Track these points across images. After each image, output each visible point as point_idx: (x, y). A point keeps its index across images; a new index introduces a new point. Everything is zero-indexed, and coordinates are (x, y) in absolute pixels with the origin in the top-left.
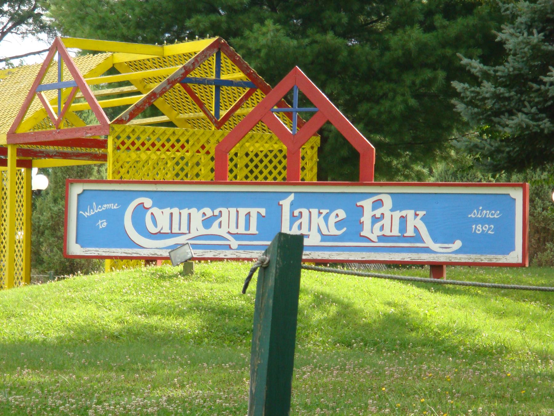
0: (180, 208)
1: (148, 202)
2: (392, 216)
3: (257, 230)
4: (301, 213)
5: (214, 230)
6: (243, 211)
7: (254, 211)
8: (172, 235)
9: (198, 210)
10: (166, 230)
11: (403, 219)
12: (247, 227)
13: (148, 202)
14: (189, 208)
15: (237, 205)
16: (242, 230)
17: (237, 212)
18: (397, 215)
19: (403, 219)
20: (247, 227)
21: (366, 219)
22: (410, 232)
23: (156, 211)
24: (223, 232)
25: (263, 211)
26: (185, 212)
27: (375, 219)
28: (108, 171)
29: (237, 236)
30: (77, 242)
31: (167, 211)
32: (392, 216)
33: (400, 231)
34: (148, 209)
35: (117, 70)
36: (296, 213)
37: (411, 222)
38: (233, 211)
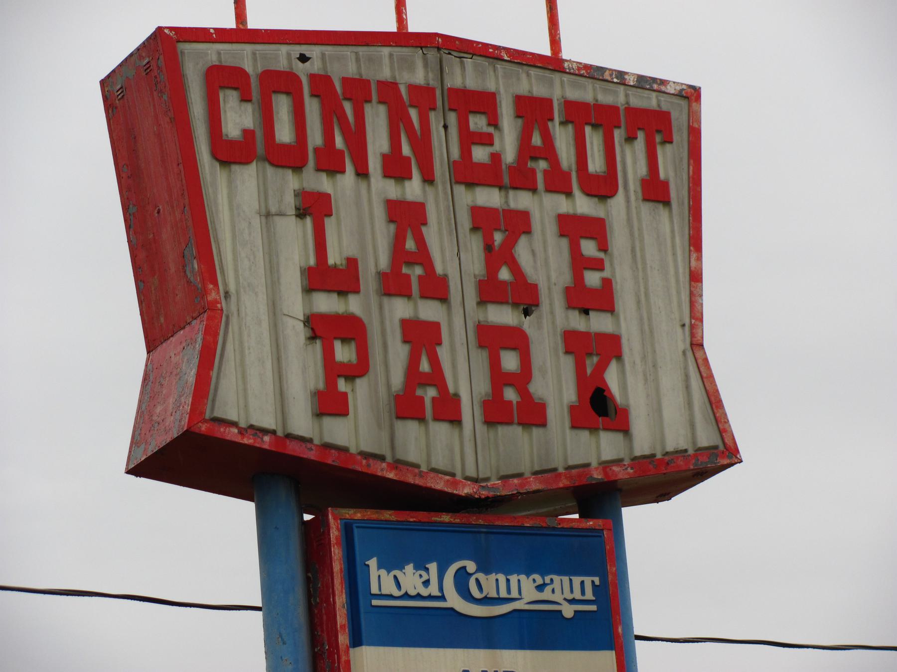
0: (507, 573)
2: (379, 576)
3: (594, 595)
4: (552, 580)
5: (546, 595)
6: (577, 580)
7: (588, 580)
9: (389, 572)
10: (494, 594)
12: (583, 592)
14: (519, 574)
16: (577, 595)
17: (571, 580)
20: (583, 592)
23: (481, 576)
24: (557, 597)
26: (514, 579)
29: (572, 601)
30: (575, 612)
31: (493, 577)
32: (379, 576)
34: (471, 575)
35: (156, 348)
38: (566, 579)
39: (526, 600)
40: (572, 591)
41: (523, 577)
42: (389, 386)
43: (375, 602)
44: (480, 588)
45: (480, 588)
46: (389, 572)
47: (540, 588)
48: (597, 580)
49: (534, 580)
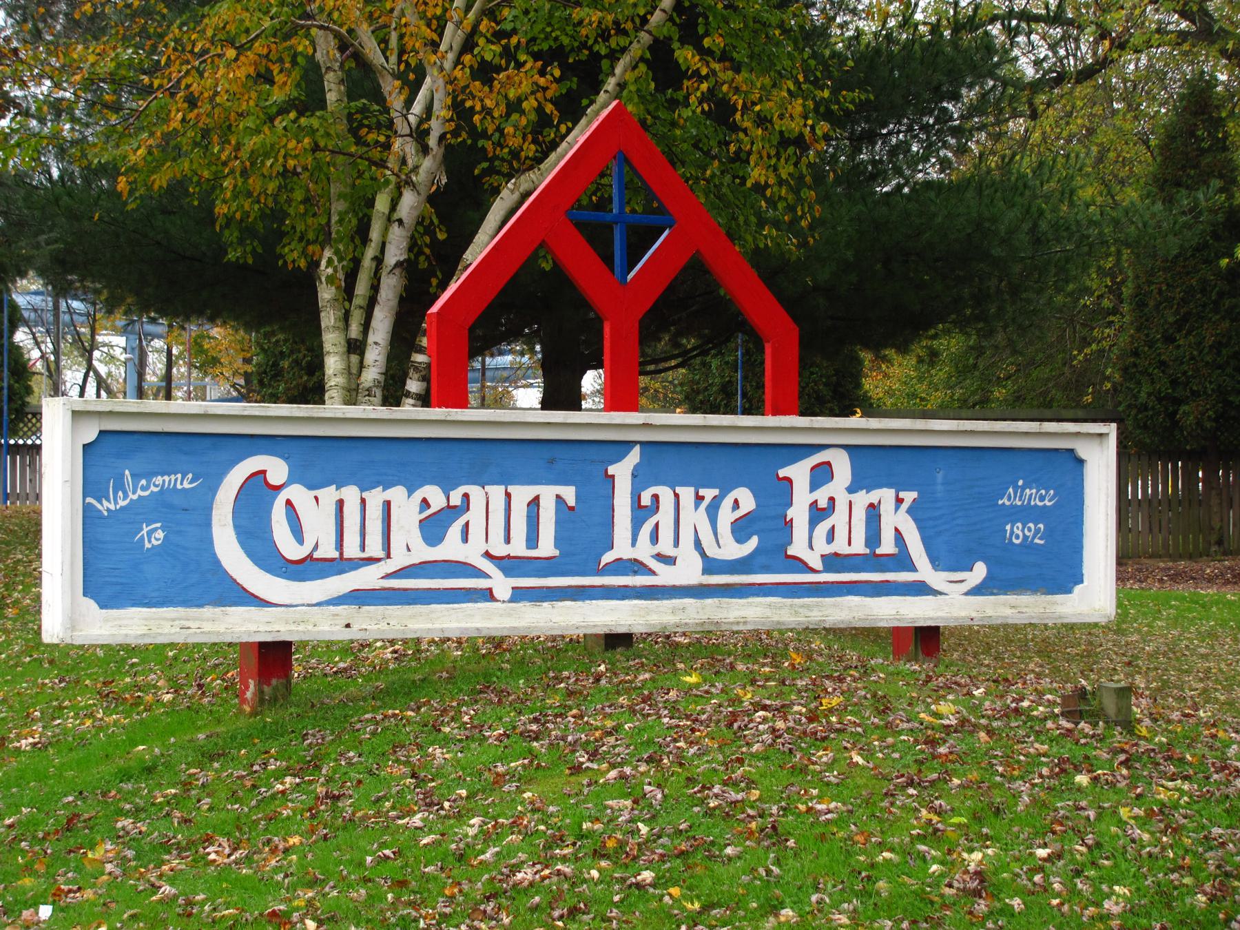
3: (556, 547)
6: (522, 494)
7: (548, 494)
8: (340, 565)
9: (410, 492)
10: (328, 550)
13: (277, 469)
17: (508, 495)
18: (862, 499)
22: (887, 546)
23: (298, 494)
24: (471, 553)
26: (376, 498)
31: (329, 495)
34: (278, 488)
39: (400, 559)
40: (508, 540)
41: (397, 494)
42: (36, 293)
43: (159, 525)
44: (298, 532)
45: (298, 532)
46: (410, 492)
47: (433, 527)
48: (569, 494)
49: (425, 503)
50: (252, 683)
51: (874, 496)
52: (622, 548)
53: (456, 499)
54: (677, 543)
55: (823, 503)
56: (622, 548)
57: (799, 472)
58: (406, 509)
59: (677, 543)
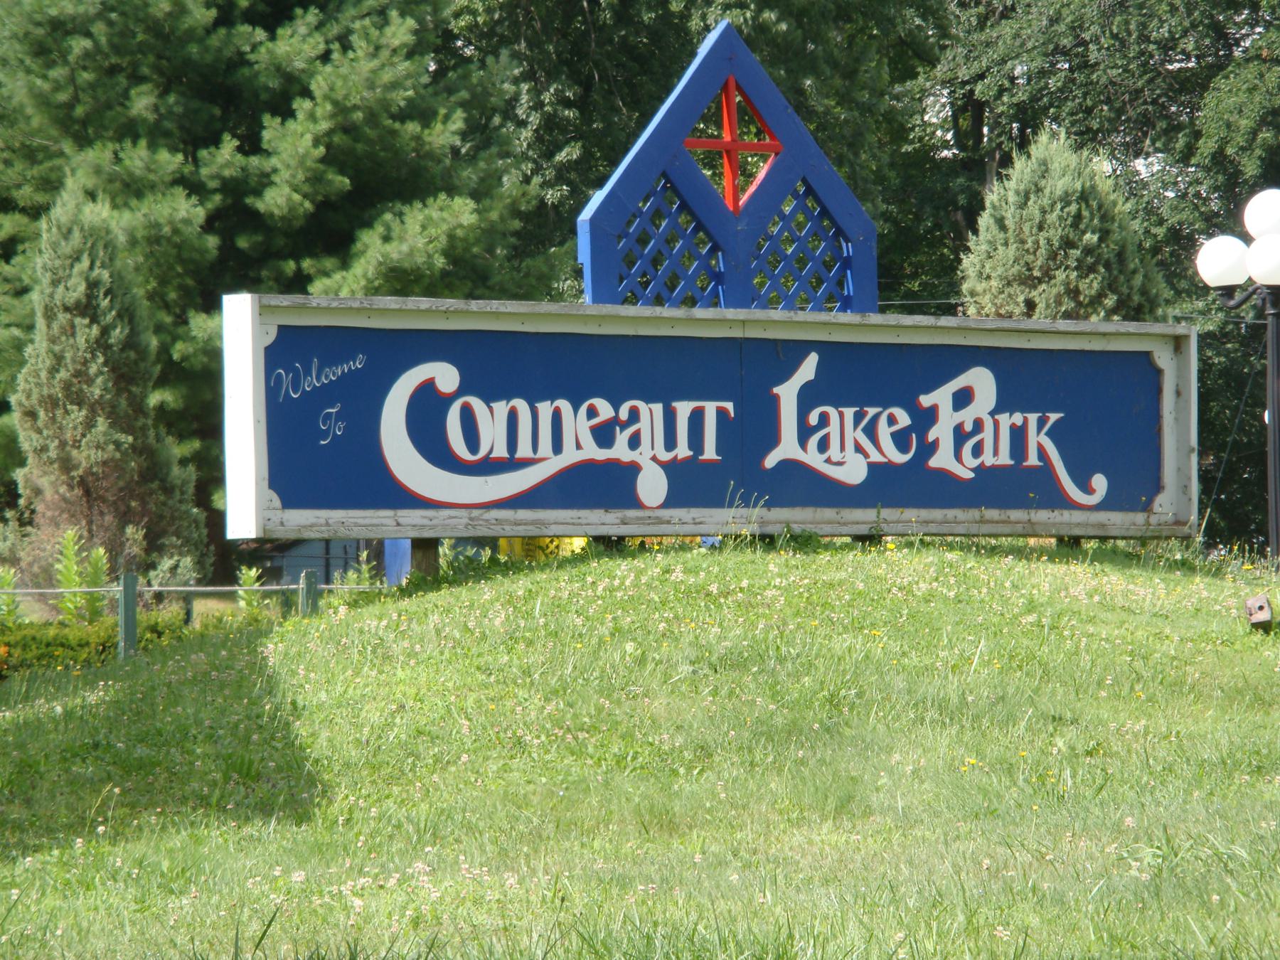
1: (446, 376)
3: (718, 454)
6: (684, 409)
7: (711, 408)
8: (512, 464)
10: (501, 451)
11: (1018, 434)
13: (446, 376)
15: (665, 395)
18: (1005, 420)
19: (1018, 434)
21: (942, 432)
22: (1033, 460)
25: (729, 406)
26: (545, 409)
27: (960, 436)
28: (614, 531)
31: (501, 408)
33: (1013, 455)
36: (813, 418)
37: (1036, 439)
50: (114, 313)
51: (1018, 418)
52: (787, 448)
53: (624, 414)
54: (843, 448)
55: (968, 427)
56: (787, 448)
57: (940, 398)
58: (577, 425)
59: (843, 448)
